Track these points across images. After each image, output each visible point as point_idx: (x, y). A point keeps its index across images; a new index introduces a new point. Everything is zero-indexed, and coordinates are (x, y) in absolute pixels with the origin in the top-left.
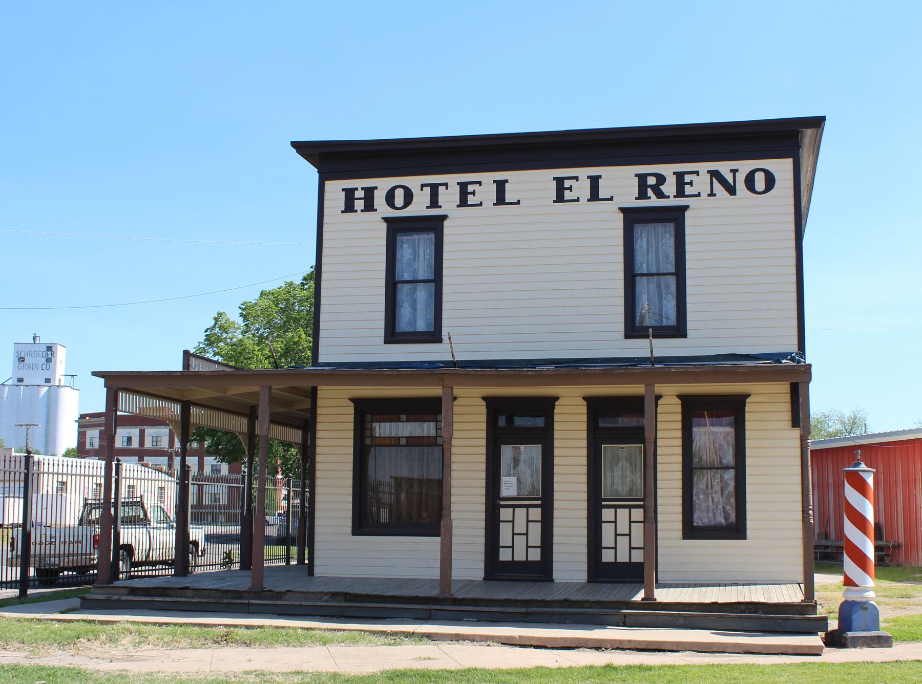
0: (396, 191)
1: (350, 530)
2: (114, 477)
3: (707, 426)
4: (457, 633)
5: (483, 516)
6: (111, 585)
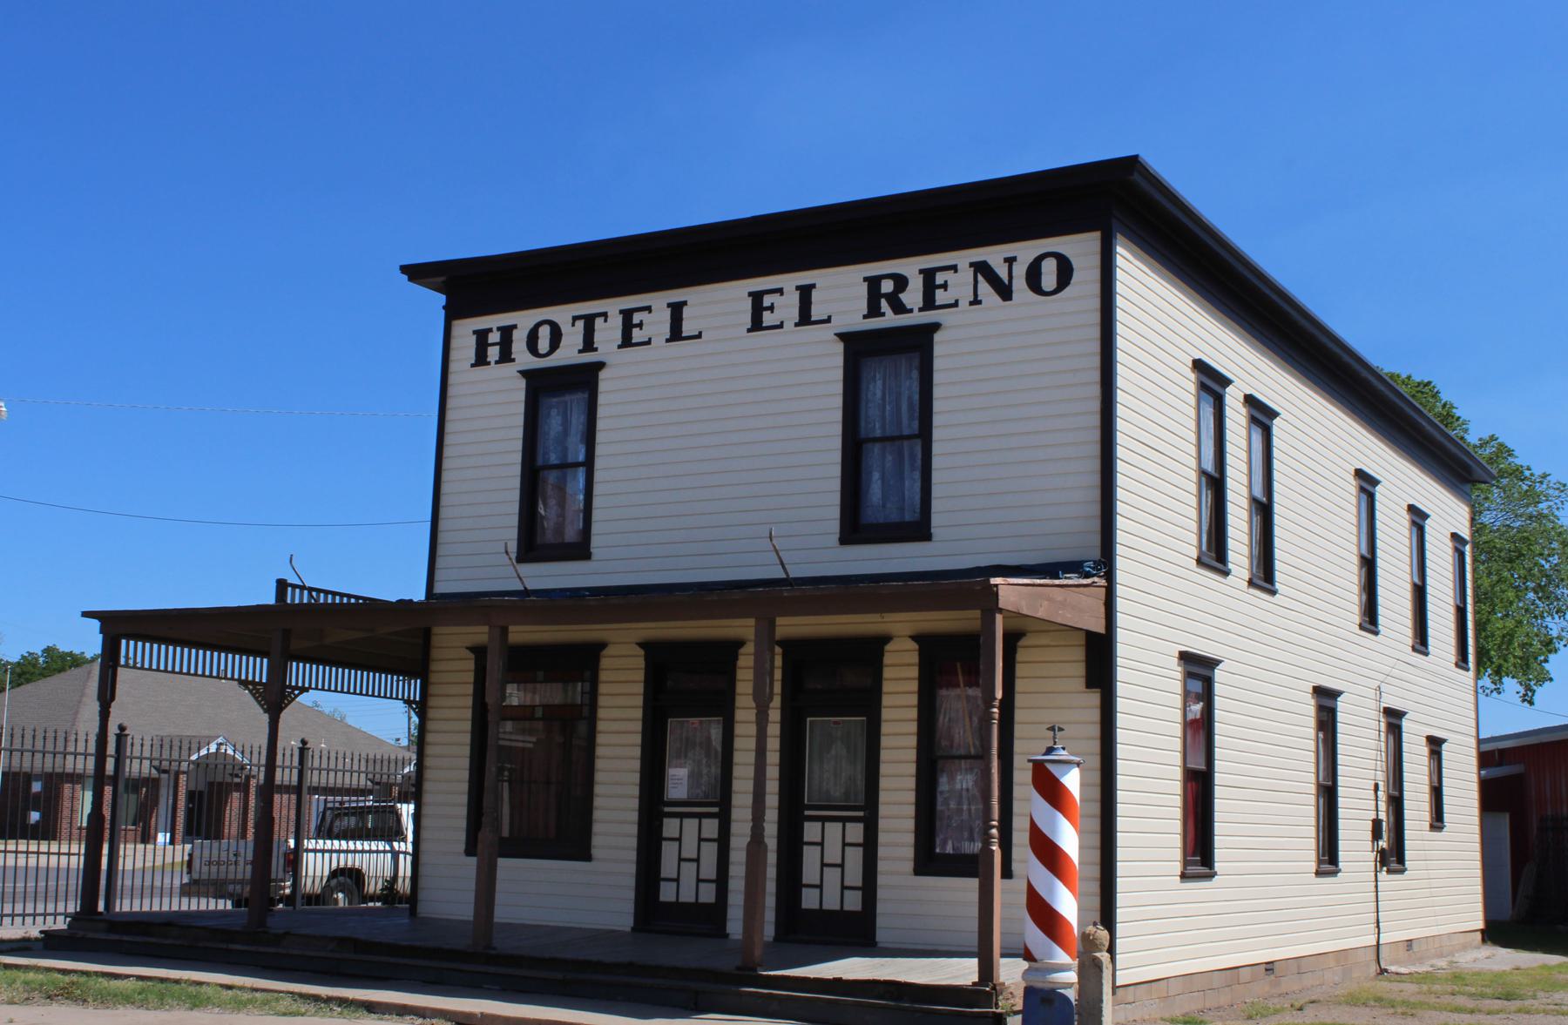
0: (1043, 263)
3: (959, 686)
4: (405, 1003)
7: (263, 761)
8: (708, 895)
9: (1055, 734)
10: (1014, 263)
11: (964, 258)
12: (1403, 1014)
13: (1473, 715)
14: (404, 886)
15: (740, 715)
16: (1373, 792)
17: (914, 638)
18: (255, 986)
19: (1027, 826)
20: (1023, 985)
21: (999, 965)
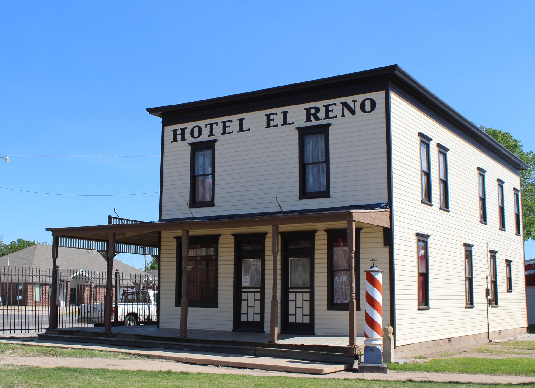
1: (174, 304)
2: (114, 279)
3: (341, 246)
5: (232, 297)
6: (55, 329)
7: (106, 277)
8: (258, 318)
9: (373, 262)
10: (356, 102)
11: (339, 101)
12: (495, 355)
13: (522, 252)
14: (154, 318)
15: (267, 258)
16: (486, 280)
17: (325, 231)
18: (110, 350)
19: (365, 293)
20: (364, 345)
21: (356, 339)
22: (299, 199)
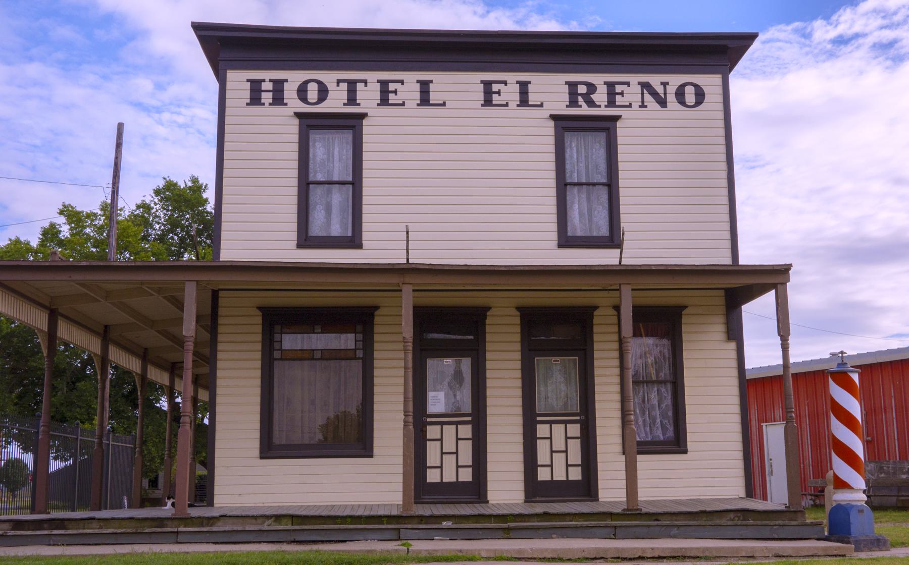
11: (635, 79)
22: (559, 248)
